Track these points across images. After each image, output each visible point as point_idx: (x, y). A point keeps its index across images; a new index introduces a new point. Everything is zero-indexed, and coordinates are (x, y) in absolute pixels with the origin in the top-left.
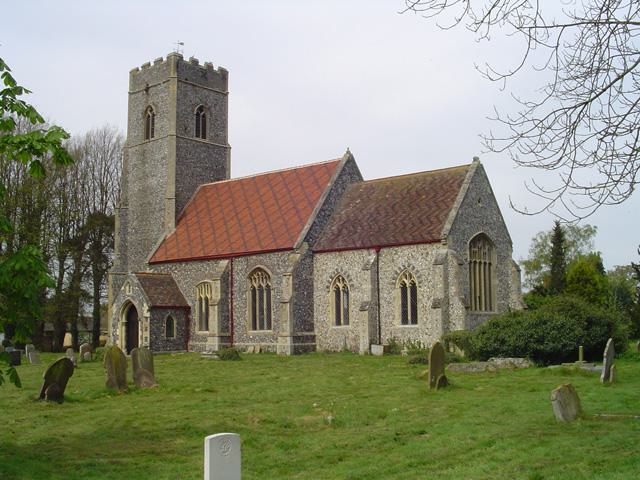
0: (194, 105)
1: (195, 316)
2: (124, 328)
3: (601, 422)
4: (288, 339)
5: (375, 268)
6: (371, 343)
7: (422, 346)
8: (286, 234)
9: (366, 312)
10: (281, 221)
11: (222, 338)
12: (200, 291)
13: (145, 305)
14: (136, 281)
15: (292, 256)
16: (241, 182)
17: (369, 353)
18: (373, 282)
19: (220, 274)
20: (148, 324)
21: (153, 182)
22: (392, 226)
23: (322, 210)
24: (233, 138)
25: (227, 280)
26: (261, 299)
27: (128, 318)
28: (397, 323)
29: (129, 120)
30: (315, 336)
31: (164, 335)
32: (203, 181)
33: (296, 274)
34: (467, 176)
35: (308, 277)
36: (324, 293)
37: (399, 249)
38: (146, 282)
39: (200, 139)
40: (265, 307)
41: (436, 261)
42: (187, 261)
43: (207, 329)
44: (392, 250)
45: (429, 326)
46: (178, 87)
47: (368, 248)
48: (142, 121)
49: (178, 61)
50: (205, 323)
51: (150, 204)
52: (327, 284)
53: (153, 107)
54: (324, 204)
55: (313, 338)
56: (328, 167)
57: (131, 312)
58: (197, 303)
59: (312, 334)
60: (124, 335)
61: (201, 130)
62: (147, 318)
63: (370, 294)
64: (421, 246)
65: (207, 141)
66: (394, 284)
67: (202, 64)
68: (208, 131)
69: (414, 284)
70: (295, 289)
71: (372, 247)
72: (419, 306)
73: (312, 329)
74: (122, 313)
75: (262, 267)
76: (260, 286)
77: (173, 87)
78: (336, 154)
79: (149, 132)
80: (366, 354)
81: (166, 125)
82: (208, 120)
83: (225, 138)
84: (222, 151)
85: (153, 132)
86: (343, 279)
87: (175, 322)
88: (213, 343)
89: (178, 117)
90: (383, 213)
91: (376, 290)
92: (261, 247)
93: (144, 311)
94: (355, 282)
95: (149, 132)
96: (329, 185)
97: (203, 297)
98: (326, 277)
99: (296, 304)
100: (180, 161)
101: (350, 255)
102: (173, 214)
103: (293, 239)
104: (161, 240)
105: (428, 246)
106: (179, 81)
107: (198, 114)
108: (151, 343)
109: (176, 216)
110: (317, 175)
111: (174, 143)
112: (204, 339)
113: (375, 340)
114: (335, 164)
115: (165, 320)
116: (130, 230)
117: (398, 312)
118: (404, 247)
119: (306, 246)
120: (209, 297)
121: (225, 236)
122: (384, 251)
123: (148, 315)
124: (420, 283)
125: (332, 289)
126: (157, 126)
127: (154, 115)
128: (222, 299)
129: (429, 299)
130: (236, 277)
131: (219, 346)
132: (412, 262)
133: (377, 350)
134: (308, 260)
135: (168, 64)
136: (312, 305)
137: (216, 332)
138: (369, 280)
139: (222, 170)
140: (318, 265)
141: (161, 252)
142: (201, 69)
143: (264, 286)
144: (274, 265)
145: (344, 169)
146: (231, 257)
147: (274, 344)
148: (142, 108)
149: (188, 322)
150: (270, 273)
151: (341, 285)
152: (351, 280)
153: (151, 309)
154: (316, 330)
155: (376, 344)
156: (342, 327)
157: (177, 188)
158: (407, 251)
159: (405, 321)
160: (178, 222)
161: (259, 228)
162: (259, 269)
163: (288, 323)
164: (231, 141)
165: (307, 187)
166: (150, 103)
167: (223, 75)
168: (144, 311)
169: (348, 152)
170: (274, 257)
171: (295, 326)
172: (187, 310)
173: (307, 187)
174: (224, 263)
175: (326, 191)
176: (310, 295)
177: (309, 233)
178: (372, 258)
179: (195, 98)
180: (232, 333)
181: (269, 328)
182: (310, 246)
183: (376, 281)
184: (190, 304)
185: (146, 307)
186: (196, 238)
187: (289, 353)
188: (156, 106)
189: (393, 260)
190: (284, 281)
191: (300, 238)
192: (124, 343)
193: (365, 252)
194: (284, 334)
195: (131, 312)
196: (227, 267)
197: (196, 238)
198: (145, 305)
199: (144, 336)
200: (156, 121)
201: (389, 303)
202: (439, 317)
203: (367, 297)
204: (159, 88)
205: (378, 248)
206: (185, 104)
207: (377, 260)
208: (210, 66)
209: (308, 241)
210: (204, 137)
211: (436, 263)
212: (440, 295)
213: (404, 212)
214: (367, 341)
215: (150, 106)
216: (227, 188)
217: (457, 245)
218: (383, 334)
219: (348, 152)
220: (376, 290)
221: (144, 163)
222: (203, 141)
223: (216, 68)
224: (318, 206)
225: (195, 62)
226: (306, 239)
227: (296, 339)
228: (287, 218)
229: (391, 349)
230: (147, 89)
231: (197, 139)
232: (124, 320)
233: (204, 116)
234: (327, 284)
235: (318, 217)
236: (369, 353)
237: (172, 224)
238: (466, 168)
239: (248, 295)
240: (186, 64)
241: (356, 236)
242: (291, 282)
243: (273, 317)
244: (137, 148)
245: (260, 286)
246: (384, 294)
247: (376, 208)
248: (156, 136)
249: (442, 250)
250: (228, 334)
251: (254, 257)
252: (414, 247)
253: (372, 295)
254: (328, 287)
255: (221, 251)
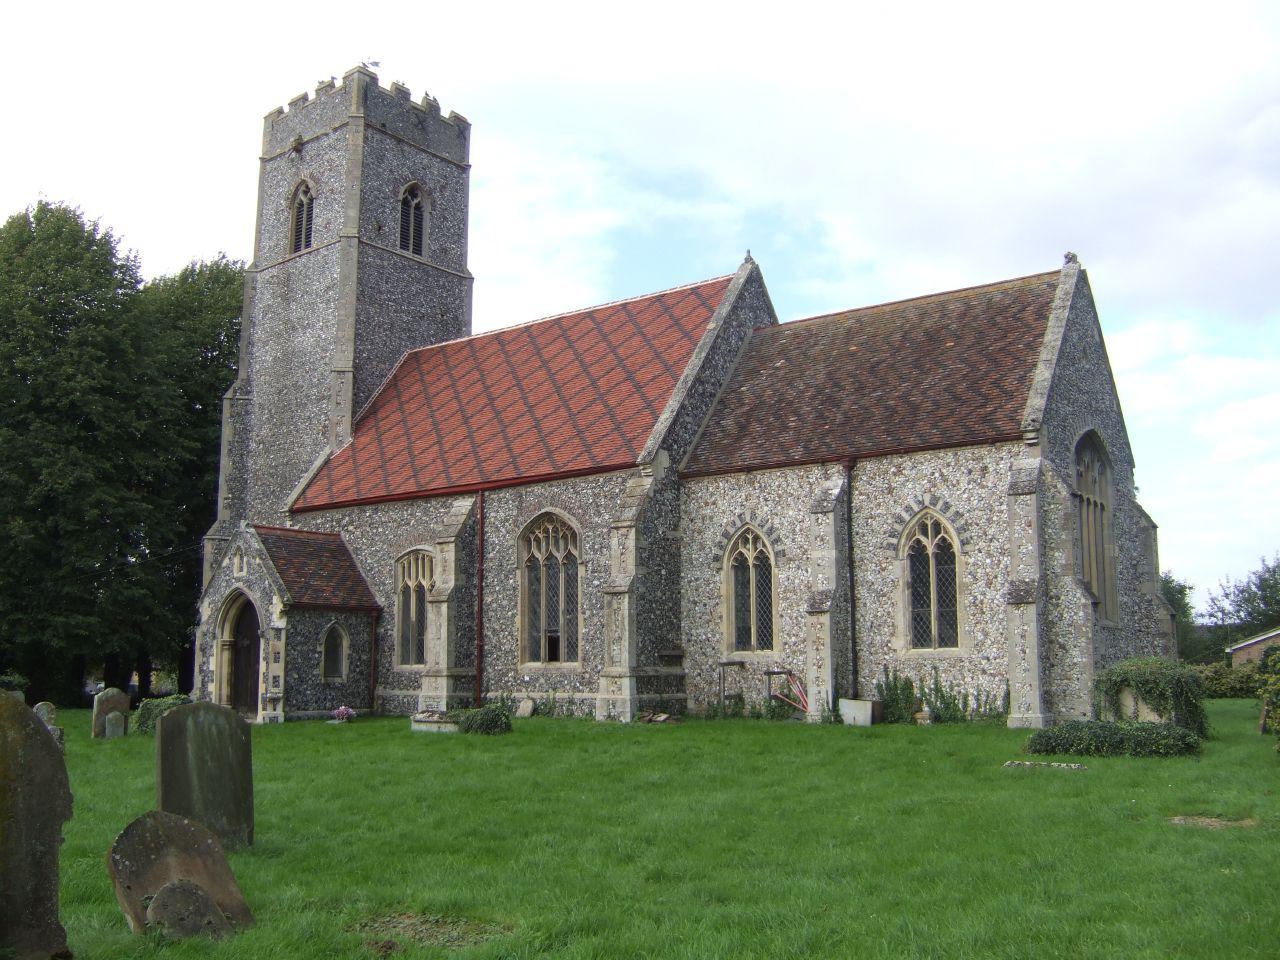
0: (396, 182)
1: (394, 630)
2: (226, 655)
3: (1196, 840)
4: (626, 683)
5: (845, 509)
6: (838, 693)
7: (972, 703)
8: (615, 434)
9: (825, 619)
10: (599, 408)
11: (456, 679)
12: (406, 572)
13: (276, 599)
14: (256, 545)
15: (630, 483)
16: (499, 339)
17: (834, 716)
18: (839, 542)
19: (454, 530)
20: (281, 645)
21: (305, 340)
22: (878, 412)
23: (698, 380)
24: (477, 260)
25: (471, 544)
26: (553, 589)
27: (237, 631)
28: (901, 642)
29: (260, 214)
30: (682, 677)
31: (319, 671)
32: (413, 340)
33: (644, 525)
34: (1059, 293)
35: (670, 535)
36: (707, 574)
37: (906, 462)
38: (283, 550)
39: (409, 254)
40: (562, 606)
41: (1013, 486)
42: (376, 502)
43: (421, 659)
44: (889, 465)
45: (993, 652)
46: (366, 139)
47: (823, 462)
48: (287, 217)
49: (366, 85)
50: (416, 649)
51: (297, 387)
52: (715, 551)
53: (311, 184)
54: (703, 368)
55: (680, 681)
56: (702, 296)
57: (244, 619)
58: (397, 600)
59: (675, 670)
60: (226, 670)
61: (412, 235)
62: (278, 630)
63: (832, 572)
64: (967, 453)
65: (423, 259)
66: (895, 548)
67: (417, 98)
68: (426, 241)
69: (945, 549)
70: (641, 562)
71: (838, 460)
72: (963, 601)
73: (677, 659)
74: (227, 612)
75: (557, 511)
76: (550, 557)
77: (355, 137)
78: (723, 265)
79: (301, 236)
80: (825, 720)
81: (336, 218)
82: (426, 216)
83: (462, 257)
84: (461, 282)
85: (308, 236)
86: (756, 538)
87: (346, 643)
88: (435, 692)
89: (363, 200)
90: (848, 384)
91: (848, 562)
92: (553, 463)
93: (274, 615)
94: (787, 544)
95: (301, 236)
96: (711, 325)
97: (412, 584)
98: (712, 535)
99: (642, 597)
100: (366, 293)
101: (774, 479)
102: (347, 406)
103: (631, 444)
104: (318, 463)
105: (984, 451)
106: (367, 126)
107: (405, 203)
108: (287, 691)
109: (354, 413)
110: (677, 312)
111: (354, 253)
112: (414, 682)
113: (847, 684)
114: (720, 287)
115: (323, 637)
116: (253, 445)
117: (902, 618)
118: (919, 457)
119: (664, 459)
120: (426, 583)
121: (467, 446)
122: (868, 466)
123: (280, 623)
124: (963, 543)
125: (727, 563)
126: (318, 222)
127: (311, 200)
128: (457, 589)
129: (989, 584)
130: (492, 538)
131: (450, 698)
132: (943, 491)
133: (856, 712)
134: (669, 495)
135: (345, 89)
136: (677, 603)
137: (443, 665)
138: (831, 539)
139: (455, 315)
140: (693, 506)
141: (323, 483)
142: (415, 108)
143: (560, 556)
144: (585, 509)
145: (740, 297)
146: (482, 489)
147: (586, 695)
148: (286, 188)
149: (377, 643)
150: (574, 524)
151: (750, 555)
152: (777, 541)
153: (289, 611)
154: (687, 663)
155: (845, 696)
156: (565, 665)
157: (357, 353)
158: (928, 465)
159: (920, 637)
160: (357, 427)
161: (547, 426)
162: (549, 517)
163: (626, 643)
164: (473, 265)
165: (655, 337)
166: (305, 174)
167: (460, 129)
168: (274, 615)
169: (749, 260)
170: (586, 487)
171: (639, 652)
172: (375, 615)
173: (655, 337)
174: (463, 505)
175: (706, 339)
176: (674, 577)
177: (671, 430)
178: (835, 483)
179: (401, 164)
180: (481, 670)
181: (572, 655)
182: (674, 460)
183: (846, 541)
184: (381, 601)
185: (277, 605)
186: (399, 453)
187: (626, 718)
188: (317, 181)
189: (890, 490)
190: (614, 542)
191: (651, 442)
192: (225, 691)
193: (816, 471)
194: (616, 670)
195: (244, 619)
196: (471, 514)
197: (399, 453)
198: (276, 599)
199: (270, 670)
200: (316, 211)
201: (881, 595)
202: (1032, 629)
203: (825, 579)
204: (325, 142)
205: (851, 464)
206: (378, 175)
207: (848, 492)
208: (432, 107)
209: (669, 449)
210: (418, 250)
211: (1015, 491)
212: (1029, 572)
213: (902, 379)
214: (827, 687)
215: (303, 182)
216: (465, 352)
217: (1054, 450)
218: (864, 671)
219: (749, 260)
220: (848, 562)
221: (286, 299)
222: (417, 258)
223: (445, 113)
224: (690, 369)
225: (402, 93)
226: (666, 444)
227: (642, 682)
228: (612, 402)
229: (894, 706)
230: (299, 147)
231: (405, 253)
232: (227, 636)
233: (418, 207)
234: (715, 551)
235: (690, 395)
236: (834, 716)
237: (345, 428)
238: (1050, 280)
239: (518, 579)
240: (382, 94)
241: (786, 438)
242: (631, 542)
243: (582, 630)
244: (274, 271)
245: (550, 557)
246: (867, 574)
247: (829, 374)
248: (314, 245)
249: (1029, 460)
250: (473, 671)
251: (537, 489)
252: (949, 456)
253: (839, 576)
254: (717, 559)
255: (457, 478)
